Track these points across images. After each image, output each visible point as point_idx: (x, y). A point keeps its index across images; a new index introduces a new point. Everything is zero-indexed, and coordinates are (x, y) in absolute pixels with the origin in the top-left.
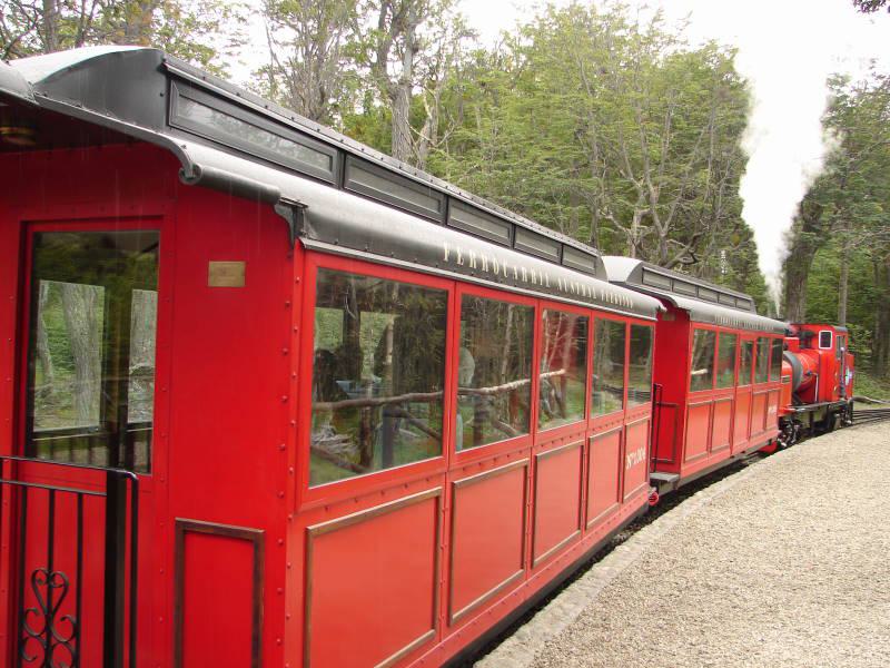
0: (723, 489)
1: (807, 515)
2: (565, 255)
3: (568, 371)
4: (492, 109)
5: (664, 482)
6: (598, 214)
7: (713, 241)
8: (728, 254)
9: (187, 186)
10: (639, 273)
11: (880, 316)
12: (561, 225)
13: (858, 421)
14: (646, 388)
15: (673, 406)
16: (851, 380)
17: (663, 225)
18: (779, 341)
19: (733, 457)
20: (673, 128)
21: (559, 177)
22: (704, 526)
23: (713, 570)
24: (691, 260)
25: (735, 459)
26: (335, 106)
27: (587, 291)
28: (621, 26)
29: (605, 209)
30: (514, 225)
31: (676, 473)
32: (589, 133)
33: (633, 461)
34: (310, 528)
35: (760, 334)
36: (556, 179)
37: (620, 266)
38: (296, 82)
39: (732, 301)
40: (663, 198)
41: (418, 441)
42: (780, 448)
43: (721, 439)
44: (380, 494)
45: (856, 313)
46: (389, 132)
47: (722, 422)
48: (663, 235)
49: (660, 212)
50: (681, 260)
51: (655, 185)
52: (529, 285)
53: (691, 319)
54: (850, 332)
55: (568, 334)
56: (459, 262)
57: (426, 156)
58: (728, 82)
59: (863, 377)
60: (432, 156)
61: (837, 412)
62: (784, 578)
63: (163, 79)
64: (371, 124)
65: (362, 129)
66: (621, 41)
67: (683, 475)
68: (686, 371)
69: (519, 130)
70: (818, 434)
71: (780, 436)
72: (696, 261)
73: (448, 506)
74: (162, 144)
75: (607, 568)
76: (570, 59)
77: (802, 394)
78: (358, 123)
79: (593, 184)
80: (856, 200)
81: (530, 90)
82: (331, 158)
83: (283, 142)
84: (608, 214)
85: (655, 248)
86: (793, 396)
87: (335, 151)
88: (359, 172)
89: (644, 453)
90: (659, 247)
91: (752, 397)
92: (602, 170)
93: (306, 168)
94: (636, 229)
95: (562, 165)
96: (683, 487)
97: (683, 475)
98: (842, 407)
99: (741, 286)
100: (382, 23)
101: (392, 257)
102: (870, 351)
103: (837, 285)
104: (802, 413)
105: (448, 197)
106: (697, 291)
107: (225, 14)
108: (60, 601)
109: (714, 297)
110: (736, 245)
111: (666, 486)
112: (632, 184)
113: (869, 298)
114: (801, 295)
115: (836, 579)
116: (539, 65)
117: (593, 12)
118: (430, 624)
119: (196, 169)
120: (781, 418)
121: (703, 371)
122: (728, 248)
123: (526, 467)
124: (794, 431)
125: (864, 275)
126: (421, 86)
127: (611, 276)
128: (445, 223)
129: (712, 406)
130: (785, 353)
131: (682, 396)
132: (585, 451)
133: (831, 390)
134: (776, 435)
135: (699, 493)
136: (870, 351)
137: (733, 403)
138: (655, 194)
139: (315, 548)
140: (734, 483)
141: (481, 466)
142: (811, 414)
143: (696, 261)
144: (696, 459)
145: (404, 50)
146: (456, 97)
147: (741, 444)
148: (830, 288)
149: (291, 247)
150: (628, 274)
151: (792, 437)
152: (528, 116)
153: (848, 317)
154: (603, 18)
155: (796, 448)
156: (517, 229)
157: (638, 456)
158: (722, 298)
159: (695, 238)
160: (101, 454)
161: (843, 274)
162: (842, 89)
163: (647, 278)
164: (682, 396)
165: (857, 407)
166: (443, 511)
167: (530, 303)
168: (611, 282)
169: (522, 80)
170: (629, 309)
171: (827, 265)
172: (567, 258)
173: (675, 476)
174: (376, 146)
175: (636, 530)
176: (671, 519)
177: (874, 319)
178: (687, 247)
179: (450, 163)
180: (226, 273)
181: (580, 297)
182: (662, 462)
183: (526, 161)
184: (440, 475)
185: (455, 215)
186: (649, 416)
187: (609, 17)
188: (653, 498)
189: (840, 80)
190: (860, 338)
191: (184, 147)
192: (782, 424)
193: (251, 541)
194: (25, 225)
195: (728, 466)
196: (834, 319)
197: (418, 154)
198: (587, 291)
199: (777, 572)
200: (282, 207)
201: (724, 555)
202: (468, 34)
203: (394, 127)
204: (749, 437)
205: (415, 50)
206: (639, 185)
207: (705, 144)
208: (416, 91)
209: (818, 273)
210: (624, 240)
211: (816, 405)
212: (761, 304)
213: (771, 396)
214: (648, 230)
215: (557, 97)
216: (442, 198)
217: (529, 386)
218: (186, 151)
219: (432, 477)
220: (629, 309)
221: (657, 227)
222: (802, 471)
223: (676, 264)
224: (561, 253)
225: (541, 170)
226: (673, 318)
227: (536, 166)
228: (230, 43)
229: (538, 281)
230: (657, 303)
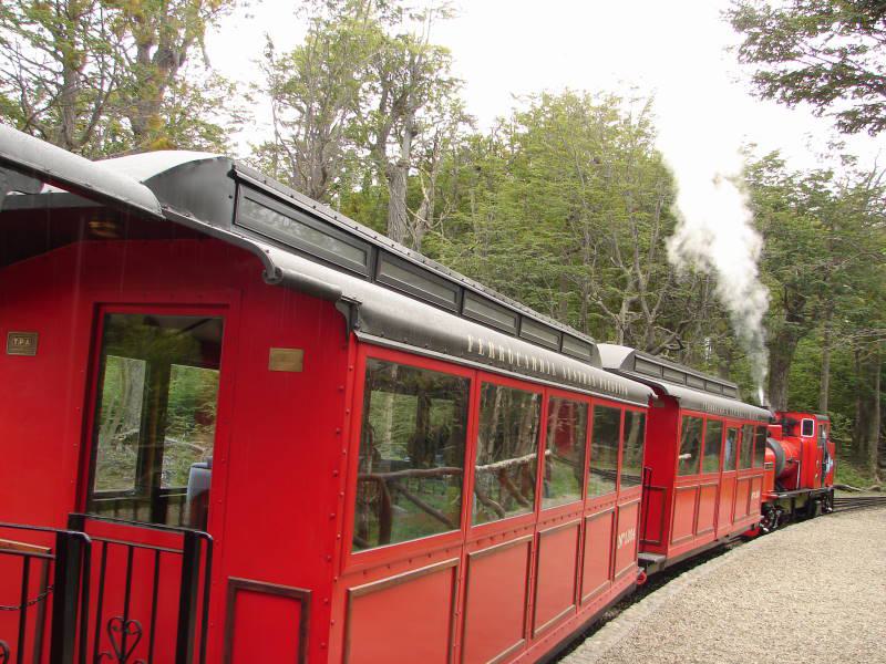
0: (707, 572)
1: (789, 598)
2: (564, 342)
3: (554, 452)
4: (488, 194)
5: (652, 562)
7: (699, 328)
8: (713, 341)
9: (271, 286)
10: (632, 361)
11: (861, 405)
12: (551, 310)
14: (637, 472)
15: (661, 489)
16: (832, 469)
17: (650, 312)
18: (762, 429)
21: (552, 263)
22: (690, 605)
23: (700, 647)
24: (677, 346)
25: (719, 543)
26: (337, 186)
27: (587, 379)
28: (614, 116)
29: (595, 294)
30: (520, 315)
34: (351, 589)
35: (745, 419)
36: (547, 265)
37: (614, 352)
38: (298, 163)
40: (652, 285)
41: (407, 516)
42: (762, 533)
43: (706, 522)
46: (385, 212)
47: (707, 506)
49: (648, 298)
50: (668, 346)
51: (644, 273)
52: (538, 373)
53: (681, 406)
54: (831, 420)
55: (555, 416)
57: (422, 236)
59: (845, 467)
60: (429, 238)
61: (819, 499)
62: (768, 657)
63: (232, 182)
64: (367, 203)
65: (358, 208)
66: (614, 132)
67: (670, 556)
68: (675, 456)
69: (515, 215)
70: (800, 520)
71: (762, 521)
72: (682, 348)
73: (463, 576)
74: (248, 247)
75: (598, 643)
76: (566, 148)
77: (784, 480)
78: (355, 202)
80: (839, 292)
81: (525, 177)
82: (366, 254)
83: (264, 211)
84: (598, 299)
85: (643, 333)
86: (776, 483)
87: (370, 247)
88: (473, 303)
89: (634, 535)
90: (646, 334)
91: (736, 483)
92: (592, 257)
93: (320, 251)
95: (551, 249)
96: (668, 568)
97: (670, 556)
98: (823, 495)
99: (725, 372)
100: (382, 107)
101: (426, 347)
102: (850, 440)
103: (818, 374)
104: (784, 498)
105: (464, 288)
106: (685, 379)
107: (230, 92)
108: (131, 652)
109: (701, 384)
110: (721, 332)
112: (620, 272)
113: (850, 387)
114: (784, 382)
115: (818, 659)
116: (535, 152)
117: (587, 102)
118: (571, 601)
119: (278, 271)
120: (763, 504)
121: (687, 456)
122: (715, 336)
123: (530, 543)
124: (777, 516)
126: (417, 167)
127: (606, 363)
128: (460, 313)
129: (698, 491)
130: (768, 440)
132: (581, 529)
135: (685, 575)
136: (850, 440)
137: (718, 488)
139: (353, 606)
142: (793, 500)
144: (682, 541)
145: (403, 133)
146: (452, 179)
147: (725, 528)
148: (811, 377)
149: (346, 339)
151: (774, 521)
153: (829, 406)
154: (596, 110)
155: (778, 533)
157: (628, 536)
160: (144, 513)
161: (825, 363)
162: (825, 184)
163: (639, 366)
164: (670, 480)
165: (838, 494)
166: (459, 578)
167: (517, 384)
168: (605, 369)
169: (515, 164)
173: (661, 557)
174: (371, 224)
175: (624, 609)
176: (658, 598)
177: (854, 408)
178: (674, 334)
179: (446, 246)
180: (286, 359)
183: (520, 246)
184: (458, 546)
185: (469, 306)
186: (639, 499)
187: (604, 109)
188: (640, 578)
189: (823, 176)
190: (841, 427)
191: (268, 251)
192: (764, 511)
193: (299, 600)
194: (98, 306)
196: (816, 409)
198: (587, 379)
199: (761, 651)
200: (342, 305)
201: (710, 633)
202: (466, 119)
203: (391, 207)
204: (733, 522)
205: (413, 134)
206: (628, 272)
208: (413, 172)
209: (802, 361)
210: (613, 325)
214: (637, 316)
215: (551, 185)
216: (458, 289)
217: (535, 461)
218: (270, 255)
219: (434, 552)
220: (604, 391)
222: (785, 555)
223: (663, 350)
224: (561, 342)
225: (534, 255)
226: (662, 405)
228: (232, 119)
230: (649, 390)
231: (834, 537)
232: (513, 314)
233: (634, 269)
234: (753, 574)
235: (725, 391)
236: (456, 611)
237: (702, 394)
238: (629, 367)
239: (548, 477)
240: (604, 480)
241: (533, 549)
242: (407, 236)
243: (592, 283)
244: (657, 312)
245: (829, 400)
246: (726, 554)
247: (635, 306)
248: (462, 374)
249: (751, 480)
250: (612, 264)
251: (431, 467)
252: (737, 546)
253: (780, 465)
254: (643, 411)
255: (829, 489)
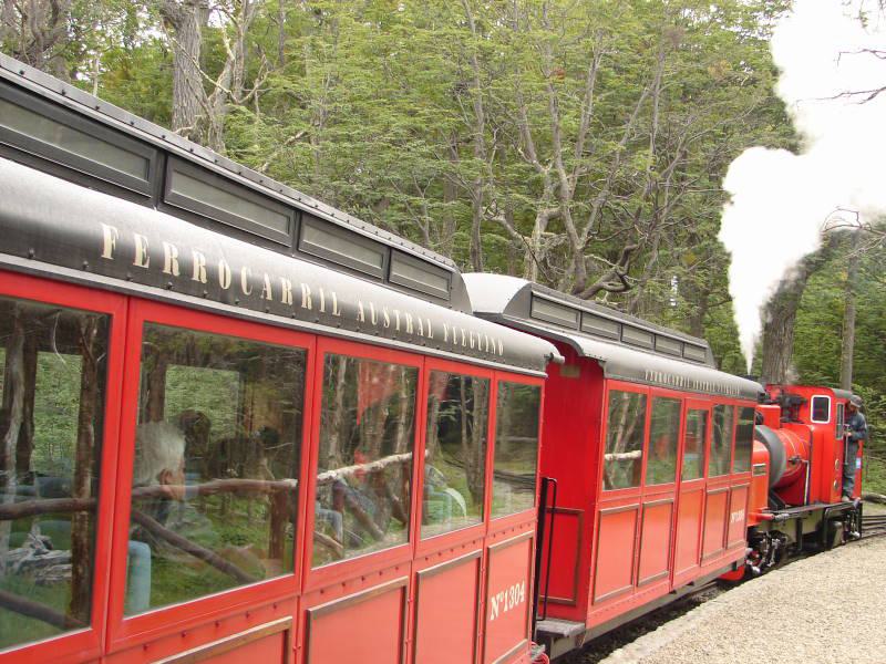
2: (395, 265)
5: (559, 636)
6: (481, 213)
10: (525, 300)
13: (871, 533)
15: (575, 514)
17: (580, 235)
18: (748, 413)
19: (674, 592)
20: (601, 86)
21: (423, 155)
24: (620, 286)
25: (678, 595)
29: (493, 206)
31: (577, 620)
32: (471, 90)
33: (501, 605)
34: (311, 610)
36: (421, 159)
37: (492, 289)
39: (677, 349)
40: (578, 193)
42: (749, 575)
43: (654, 556)
44: (179, 637)
45: (868, 370)
47: (656, 533)
48: (579, 247)
50: (606, 285)
51: (568, 172)
53: (606, 375)
56: (138, 262)
58: (686, 21)
65: (130, 72)
68: (597, 456)
70: (811, 552)
71: (750, 557)
72: (627, 288)
77: (784, 491)
79: (475, 168)
84: (497, 213)
86: (770, 495)
87: (155, 151)
89: (522, 593)
91: (705, 497)
94: (539, 239)
98: (846, 512)
99: (696, 325)
103: (839, 328)
104: (784, 520)
106: (620, 333)
109: (647, 340)
110: (690, 266)
111: (560, 642)
123: (404, 589)
125: (880, 314)
127: (477, 303)
130: (758, 428)
131: (590, 499)
133: (830, 485)
134: (744, 555)
137: (675, 508)
138: (568, 187)
139: (421, 583)
140: (674, 635)
141: (218, 628)
143: (627, 288)
144: (611, 599)
147: (688, 571)
148: (829, 333)
150: (507, 302)
152: (379, 60)
153: (853, 377)
156: (305, 219)
157: (511, 596)
158: (661, 344)
159: (628, 253)
161: (848, 311)
163: (538, 309)
168: (478, 315)
170: (496, 357)
171: (826, 298)
172: (397, 272)
173: (578, 626)
178: (616, 266)
181: (402, 334)
182: (554, 603)
183: (372, 129)
185: (179, 187)
186: (532, 531)
190: (872, 407)
192: (752, 538)
195: (669, 605)
196: (835, 379)
197: (211, 114)
204: (700, 561)
206: (546, 171)
207: (646, 112)
210: (521, 255)
211: (805, 509)
212: (725, 353)
213: (735, 495)
214: (558, 239)
220: (496, 357)
221: (569, 235)
223: (597, 291)
224: (386, 266)
226: (573, 373)
227: (389, 136)
229: (316, 303)
231: (864, 581)
232: (377, 248)
233: (554, 167)
234: (732, 649)
235: (688, 351)
236: (406, 640)
237: (649, 356)
238: (519, 313)
239: (426, 497)
240: (517, 491)
241: (409, 599)
242: (203, 116)
243: (489, 187)
244: (589, 234)
245: (854, 367)
246: (690, 613)
247: (555, 224)
248: (297, 345)
249: (729, 494)
250: (518, 158)
251: (241, 476)
252: (711, 597)
253: (778, 469)
254: (534, 384)
255: (855, 503)
